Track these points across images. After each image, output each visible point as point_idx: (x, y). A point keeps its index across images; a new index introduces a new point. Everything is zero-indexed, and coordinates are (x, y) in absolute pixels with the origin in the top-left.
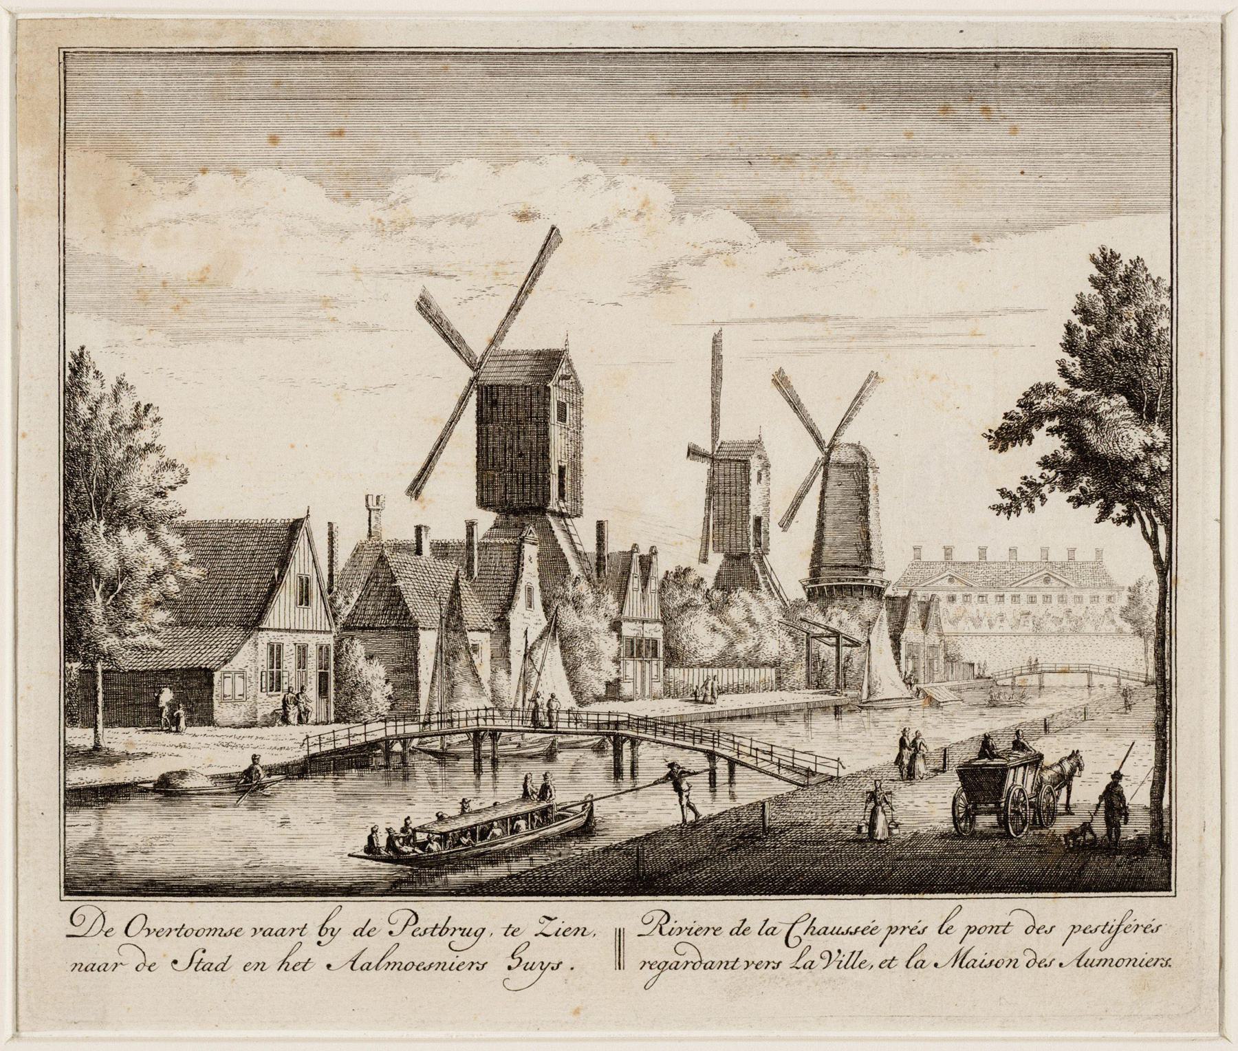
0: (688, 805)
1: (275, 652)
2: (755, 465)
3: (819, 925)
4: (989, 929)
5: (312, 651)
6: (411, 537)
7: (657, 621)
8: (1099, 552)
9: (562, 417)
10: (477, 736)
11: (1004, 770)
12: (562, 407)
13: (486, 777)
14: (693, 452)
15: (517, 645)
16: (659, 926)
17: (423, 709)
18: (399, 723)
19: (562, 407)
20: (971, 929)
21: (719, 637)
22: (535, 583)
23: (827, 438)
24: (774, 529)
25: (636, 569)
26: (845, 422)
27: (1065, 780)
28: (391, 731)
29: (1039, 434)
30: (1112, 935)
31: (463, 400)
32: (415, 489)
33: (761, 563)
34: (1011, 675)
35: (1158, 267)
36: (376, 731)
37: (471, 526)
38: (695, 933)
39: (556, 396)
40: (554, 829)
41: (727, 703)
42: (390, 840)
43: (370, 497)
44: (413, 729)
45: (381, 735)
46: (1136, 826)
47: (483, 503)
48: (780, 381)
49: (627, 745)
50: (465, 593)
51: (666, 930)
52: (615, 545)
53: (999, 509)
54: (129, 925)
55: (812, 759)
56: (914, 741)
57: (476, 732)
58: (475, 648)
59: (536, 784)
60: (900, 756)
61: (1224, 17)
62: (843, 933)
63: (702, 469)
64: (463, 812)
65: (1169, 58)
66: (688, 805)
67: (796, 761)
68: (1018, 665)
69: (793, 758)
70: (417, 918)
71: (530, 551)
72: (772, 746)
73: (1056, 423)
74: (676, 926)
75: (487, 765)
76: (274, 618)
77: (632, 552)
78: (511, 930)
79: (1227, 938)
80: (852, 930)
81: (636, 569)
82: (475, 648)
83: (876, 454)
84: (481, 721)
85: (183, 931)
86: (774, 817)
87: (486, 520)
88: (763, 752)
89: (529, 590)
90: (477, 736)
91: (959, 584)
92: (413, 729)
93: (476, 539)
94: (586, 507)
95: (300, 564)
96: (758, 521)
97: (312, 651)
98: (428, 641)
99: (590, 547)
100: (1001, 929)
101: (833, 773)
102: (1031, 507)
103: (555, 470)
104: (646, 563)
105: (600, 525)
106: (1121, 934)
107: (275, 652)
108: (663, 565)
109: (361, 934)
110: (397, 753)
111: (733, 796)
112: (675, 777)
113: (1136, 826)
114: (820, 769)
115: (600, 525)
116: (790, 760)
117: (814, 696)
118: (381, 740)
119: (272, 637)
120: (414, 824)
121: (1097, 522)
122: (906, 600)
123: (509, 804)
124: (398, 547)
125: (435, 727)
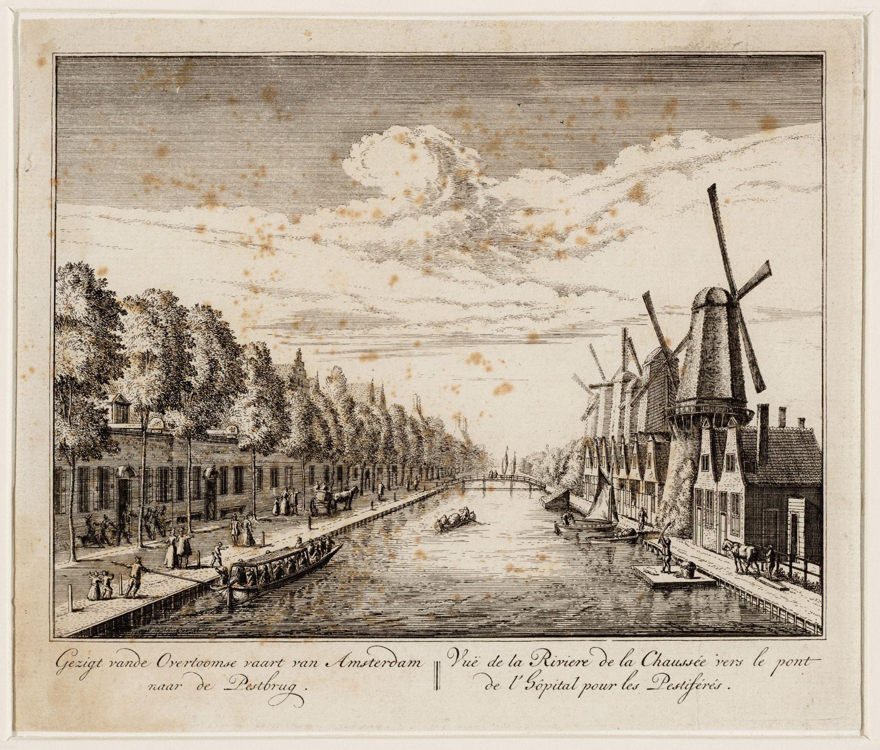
3: (662, 659)
4: (794, 662)
16: (544, 660)
20: (782, 662)
21: (80, 353)
30: (687, 690)
38: (570, 665)
51: (549, 662)
54: (159, 660)
61: (866, 18)
62: (680, 665)
65: (821, 57)
70: (550, 655)
74: (556, 660)
78: (374, 663)
79: (866, 327)
80: (688, 662)
85: (196, 663)
91: (684, 352)
100: (803, 662)
106: (694, 690)
121: (715, 185)
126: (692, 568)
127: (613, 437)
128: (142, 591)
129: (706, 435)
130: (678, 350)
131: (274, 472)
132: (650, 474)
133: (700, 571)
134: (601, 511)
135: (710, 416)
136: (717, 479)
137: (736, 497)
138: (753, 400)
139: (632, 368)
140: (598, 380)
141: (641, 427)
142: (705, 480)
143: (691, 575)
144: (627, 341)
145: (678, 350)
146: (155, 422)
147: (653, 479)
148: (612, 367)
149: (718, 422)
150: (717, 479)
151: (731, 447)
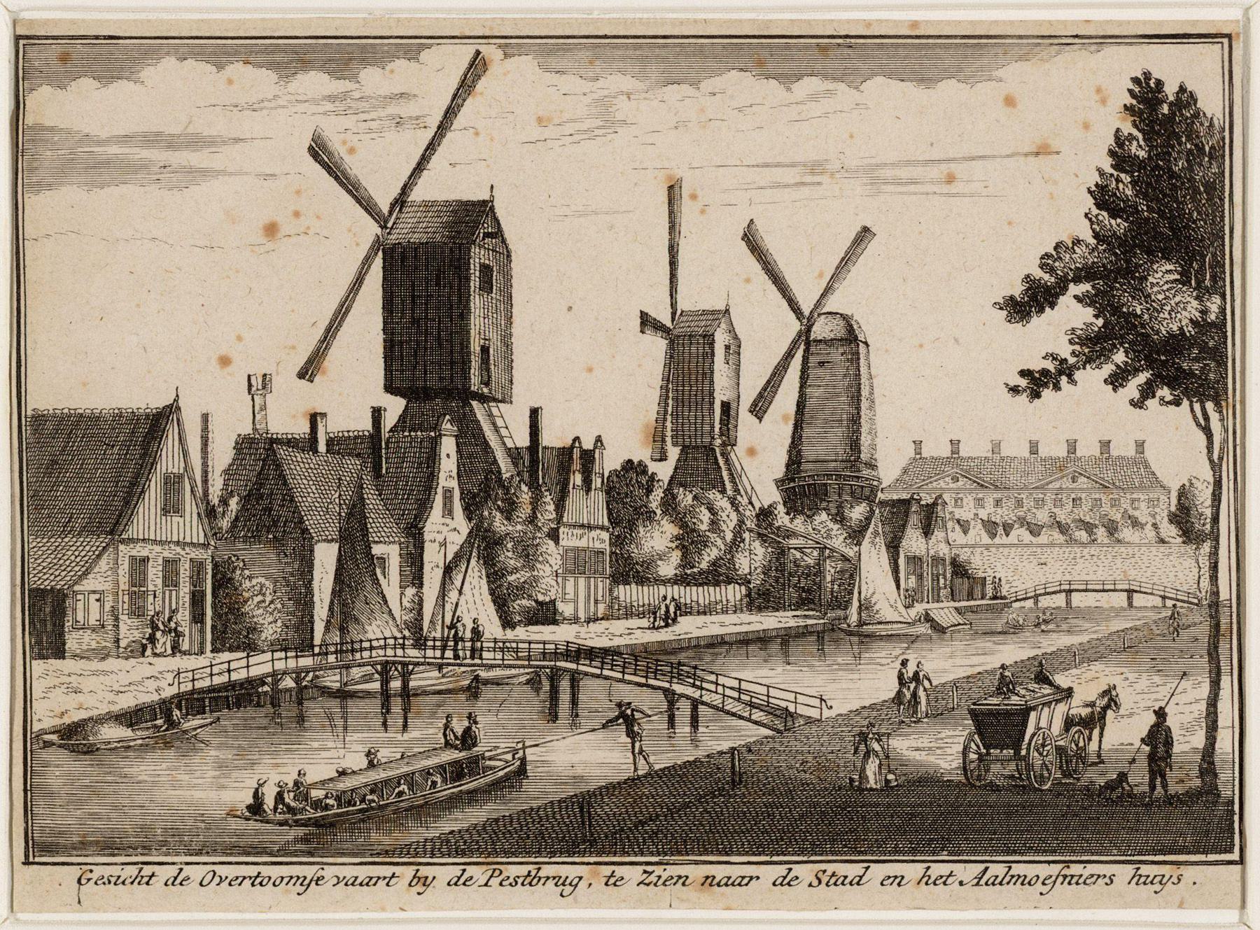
0: (641, 752)
1: (140, 564)
2: (721, 338)
5: (185, 570)
6: (303, 428)
7: (602, 528)
8: (1140, 446)
9: (487, 286)
10: (385, 670)
11: (1025, 712)
12: (486, 270)
13: (396, 720)
14: (647, 322)
15: (433, 558)
17: (317, 641)
18: (289, 654)
19: (486, 270)
22: (454, 484)
23: (806, 308)
24: (745, 418)
25: (576, 465)
26: (828, 291)
27: (1093, 721)
28: (280, 665)
29: (1066, 301)
31: (367, 262)
32: (308, 372)
33: (725, 455)
34: (1033, 594)
35: (1211, 103)
36: (261, 665)
37: (377, 413)
39: (478, 256)
40: (469, 785)
41: (689, 627)
42: (279, 798)
43: (253, 379)
44: (306, 662)
45: (267, 668)
46: (1183, 778)
47: (390, 388)
48: (751, 241)
49: (565, 684)
50: (372, 499)
52: (553, 437)
53: (1015, 390)
55: (791, 697)
56: (916, 674)
57: (385, 664)
58: (382, 560)
59: (459, 726)
60: (899, 693)
63: (657, 346)
64: (371, 765)
66: (641, 752)
67: (771, 700)
68: (1111, 578)
69: (768, 696)
71: (448, 446)
72: (740, 680)
73: (1085, 287)
75: (397, 707)
76: (136, 529)
77: (572, 447)
81: (576, 465)
82: (382, 560)
83: (868, 329)
84: (390, 652)
86: (750, 764)
87: (395, 407)
88: (731, 688)
89: (448, 494)
90: (385, 670)
92: (306, 662)
93: (385, 434)
94: (517, 390)
95: (169, 460)
96: (726, 407)
97: (185, 570)
98: (326, 557)
99: (523, 440)
101: (814, 713)
102: (1057, 387)
103: (475, 347)
104: (588, 458)
105: (534, 413)
107: (140, 564)
108: (610, 461)
109: (173, 884)
110: (289, 690)
111: (695, 742)
112: (626, 718)
113: (1183, 778)
114: (802, 710)
115: (534, 413)
116: (766, 698)
117: (796, 619)
118: (268, 675)
119: (140, 551)
120: (310, 778)
122: (906, 503)
123: (426, 754)
124: (291, 443)
125: (332, 658)
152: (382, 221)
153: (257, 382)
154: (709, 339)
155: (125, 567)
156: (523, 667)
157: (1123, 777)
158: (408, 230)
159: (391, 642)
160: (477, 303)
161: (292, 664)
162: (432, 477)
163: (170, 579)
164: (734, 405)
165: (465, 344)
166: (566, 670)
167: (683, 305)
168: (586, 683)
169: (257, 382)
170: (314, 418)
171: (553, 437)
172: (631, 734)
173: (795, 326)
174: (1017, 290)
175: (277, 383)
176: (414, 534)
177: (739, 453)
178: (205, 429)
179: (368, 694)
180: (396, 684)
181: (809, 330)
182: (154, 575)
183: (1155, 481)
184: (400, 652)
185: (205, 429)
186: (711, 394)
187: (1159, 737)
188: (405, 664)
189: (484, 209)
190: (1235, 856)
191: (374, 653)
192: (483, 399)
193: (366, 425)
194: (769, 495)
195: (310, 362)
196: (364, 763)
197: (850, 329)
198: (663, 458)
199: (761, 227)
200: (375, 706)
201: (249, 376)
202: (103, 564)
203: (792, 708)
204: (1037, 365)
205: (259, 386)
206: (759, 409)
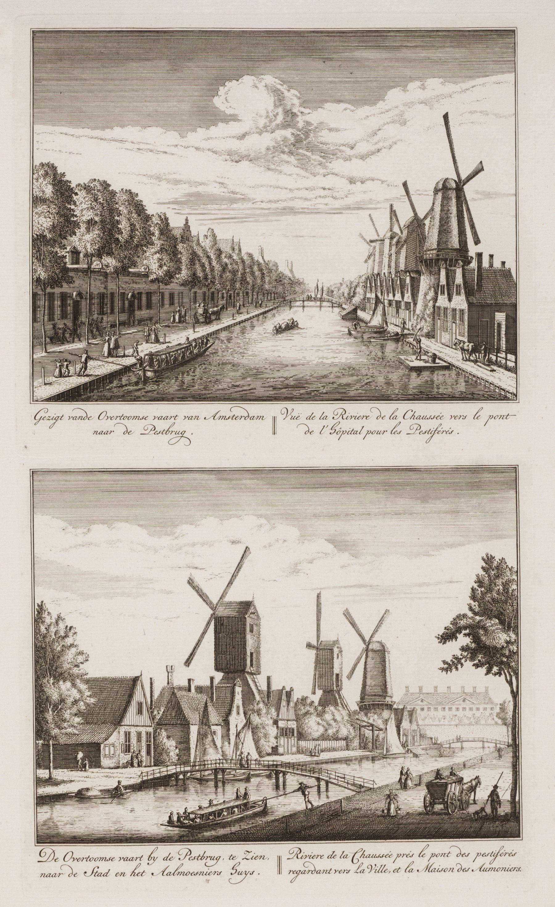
1: (127, 735)
2: (336, 650)
7: (294, 720)
9: (251, 631)
12: (252, 626)
13: (220, 790)
14: (309, 646)
15: (233, 731)
17: (192, 759)
19: (252, 626)
24: (344, 679)
25: (284, 697)
27: (473, 789)
28: (178, 770)
29: (460, 636)
31: (208, 624)
32: (188, 662)
36: (172, 770)
37: (212, 679)
45: (174, 771)
46: (504, 809)
47: (217, 669)
49: (281, 775)
52: (275, 687)
57: (216, 770)
60: (400, 779)
63: (312, 653)
71: (238, 690)
75: (220, 784)
76: (126, 721)
77: (282, 690)
81: (284, 697)
83: (389, 646)
84: (218, 765)
87: (219, 676)
92: (188, 769)
94: (262, 669)
95: (138, 696)
98: (194, 730)
99: (264, 687)
101: (371, 786)
102: (457, 669)
104: (289, 694)
105: (269, 678)
108: (296, 696)
112: (302, 789)
113: (504, 809)
115: (269, 678)
125: (197, 768)
126: (435, 357)
127: (384, 273)
128: (88, 372)
129: (443, 273)
130: (425, 218)
131: (172, 296)
132: (408, 297)
133: (440, 359)
134: (377, 321)
135: (445, 260)
136: (450, 300)
137: (462, 311)
138: (473, 250)
139: (396, 229)
140: (376, 237)
141: (402, 267)
142: (442, 301)
143: (434, 361)
144: (393, 213)
145: (425, 218)
146: (96, 264)
147: (410, 300)
148: (384, 230)
149: (452, 263)
150: (450, 300)
151: (459, 280)
152: (214, 608)
153: (169, 669)
154: (332, 650)
155: (122, 733)
156: (266, 770)
157: (483, 809)
158: (222, 612)
159: (218, 761)
160: (249, 636)
161: (182, 769)
162: (232, 701)
163: (139, 740)
164: (340, 675)
165: (245, 654)
166: (282, 771)
167: (322, 638)
168: (288, 776)
169: (169, 669)
170: (189, 680)
171: (275, 687)
172: (304, 794)
173: (365, 646)
174: (441, 631)
175: (176, 669)
176: (226, 723)
177: (343, 692)
178: (151, 684)
179: (211, 780)
180: (220, 776)
181: (368, 646)
182: (134, 740)
183: (491, 701)
184: (221, 765)
185: (151, 684)
186: (333, 672)
187: (494, 796)
188: (223, 769)
189: (460, 649)
190: (521, 838)
191: (213, 766)
192: (252, 674)
193: (208, 683)
194: (354, 707)
195: (188, 660)
196: (207, 805)
197: (383, 646)
198: (314, 693)
199: (351, 611)
200: (212, 784)
201: (167, 666)
202: (115, 733)
203: (362, 784)
204: (449, 659)
205: (170, 670)
206: (349, 677)
